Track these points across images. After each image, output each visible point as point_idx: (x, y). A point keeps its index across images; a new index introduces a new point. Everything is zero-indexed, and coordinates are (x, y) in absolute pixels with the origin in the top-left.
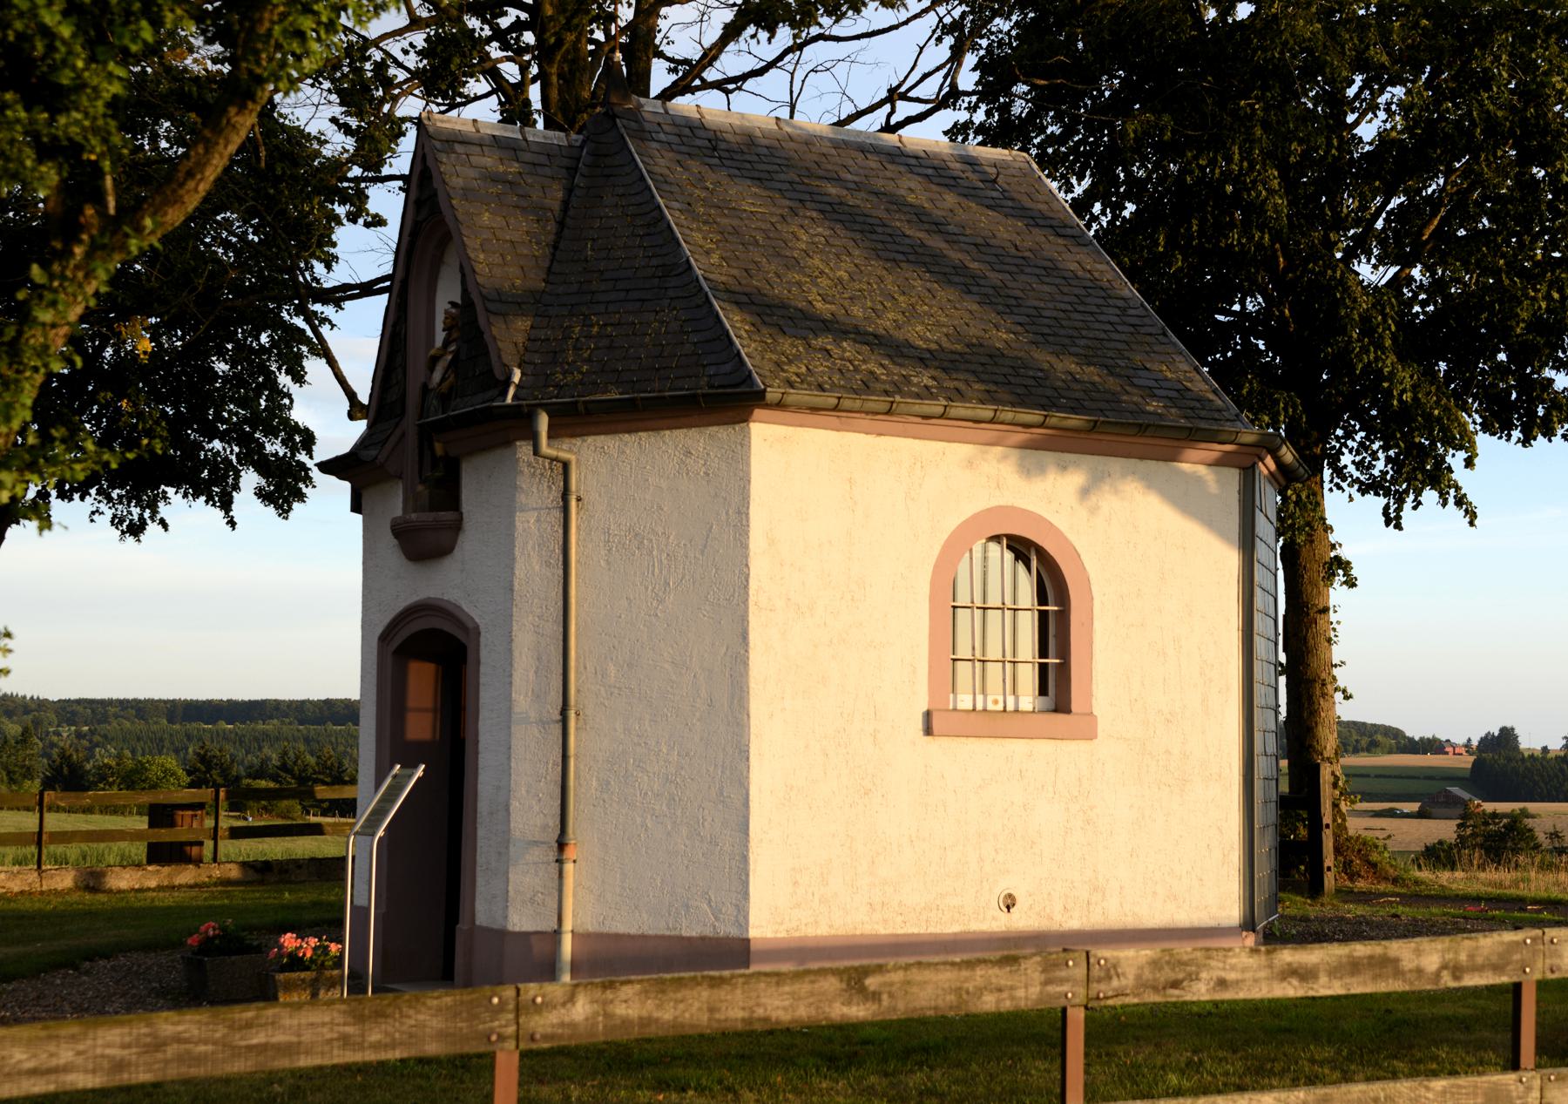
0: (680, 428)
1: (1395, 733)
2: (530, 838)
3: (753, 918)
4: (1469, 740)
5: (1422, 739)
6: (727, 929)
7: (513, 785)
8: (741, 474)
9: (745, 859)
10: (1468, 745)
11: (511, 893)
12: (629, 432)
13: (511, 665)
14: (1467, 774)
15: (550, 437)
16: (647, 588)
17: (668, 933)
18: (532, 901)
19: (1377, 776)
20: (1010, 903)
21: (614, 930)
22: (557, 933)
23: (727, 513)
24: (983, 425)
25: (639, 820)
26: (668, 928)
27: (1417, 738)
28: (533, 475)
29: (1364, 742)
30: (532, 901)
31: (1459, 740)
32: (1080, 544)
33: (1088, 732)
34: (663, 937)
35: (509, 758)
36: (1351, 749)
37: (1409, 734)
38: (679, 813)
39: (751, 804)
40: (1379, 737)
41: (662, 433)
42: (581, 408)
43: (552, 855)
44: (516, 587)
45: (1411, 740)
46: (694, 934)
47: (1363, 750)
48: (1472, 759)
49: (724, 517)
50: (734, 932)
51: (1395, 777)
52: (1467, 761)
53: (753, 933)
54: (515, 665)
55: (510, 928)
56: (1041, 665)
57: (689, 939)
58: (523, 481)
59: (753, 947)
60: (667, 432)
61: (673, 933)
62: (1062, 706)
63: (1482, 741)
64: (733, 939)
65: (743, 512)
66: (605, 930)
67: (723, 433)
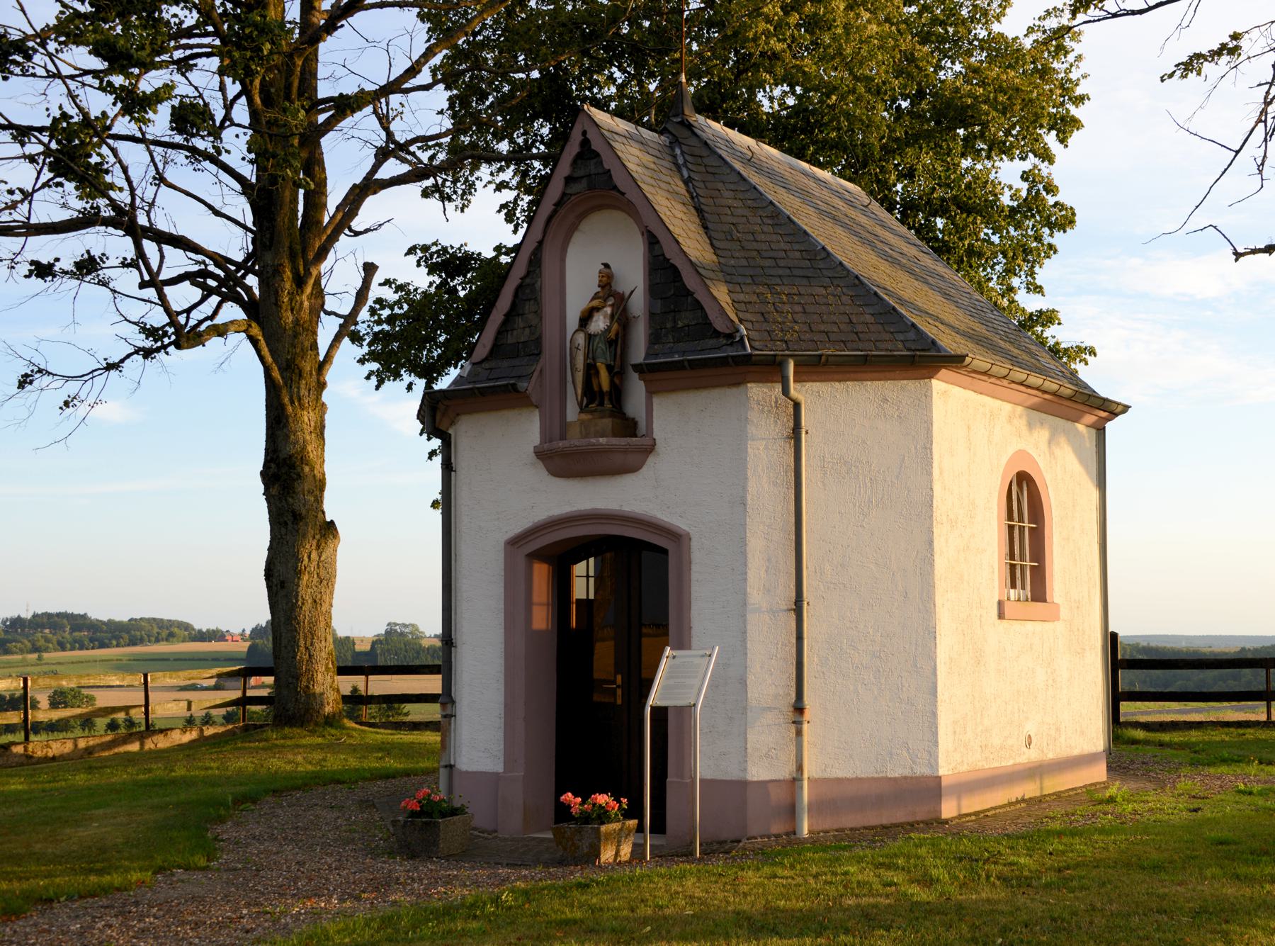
0: (880, 380)
1: (186, 627)
2: (765, 705)
3: (941, 761)
4: (244, 630)
5: (208, 631)
6: (922, 770)
7: (749, 663)
8: (926, 418)
9: (934, 714)
10: (243, 634)
11: (749, 750)
12: (839, 381)
13: (746, 565)
14: (244, 656)
15: (795, 381)
16: (855, 505)
17: (876, 775)
18: (767, 755)
19: (175, 660)
20: (1029, 742)
21: (834, 775)
22: (795, 781)
23: (916, 448)
24: (1030, 391)
25: (852, 688)
26: (877, 772)
27: (204, 630)
28: (762, 411)
29: (164, 633)
30: (767, 755)
31: (236, 630)
32: (1048, 477)
33: (1054, 617)
34: (874, 779)
35: (744, 641)
36: (153, 639)
37: (197, 627)
38: (883, 681)
39: (938, 673)
40: (176, 630)
41: (865, 383)
42: (686, 363)
43: (791, 716)
44: (749, 502)
45: (200, 631)
46: (897, 775)
47: (163, 640)
48: (248, 644)
49: (913, 451)
50: (926, 771)
51: (190, 660)
52: (244, 647)
53: (942, 771)
54: (749, 565)
55: (749, 778)
56: (1011, 565)
57: (895, 779)
58: (753, 415)
59: (944, 783)
60: (869, 383)
61: (880, 775)
62: (1039, 594)
63: (253, 631)
64: (926, 777)
65: (927, 449)
66: (827, 775)
67: (911, 385)
